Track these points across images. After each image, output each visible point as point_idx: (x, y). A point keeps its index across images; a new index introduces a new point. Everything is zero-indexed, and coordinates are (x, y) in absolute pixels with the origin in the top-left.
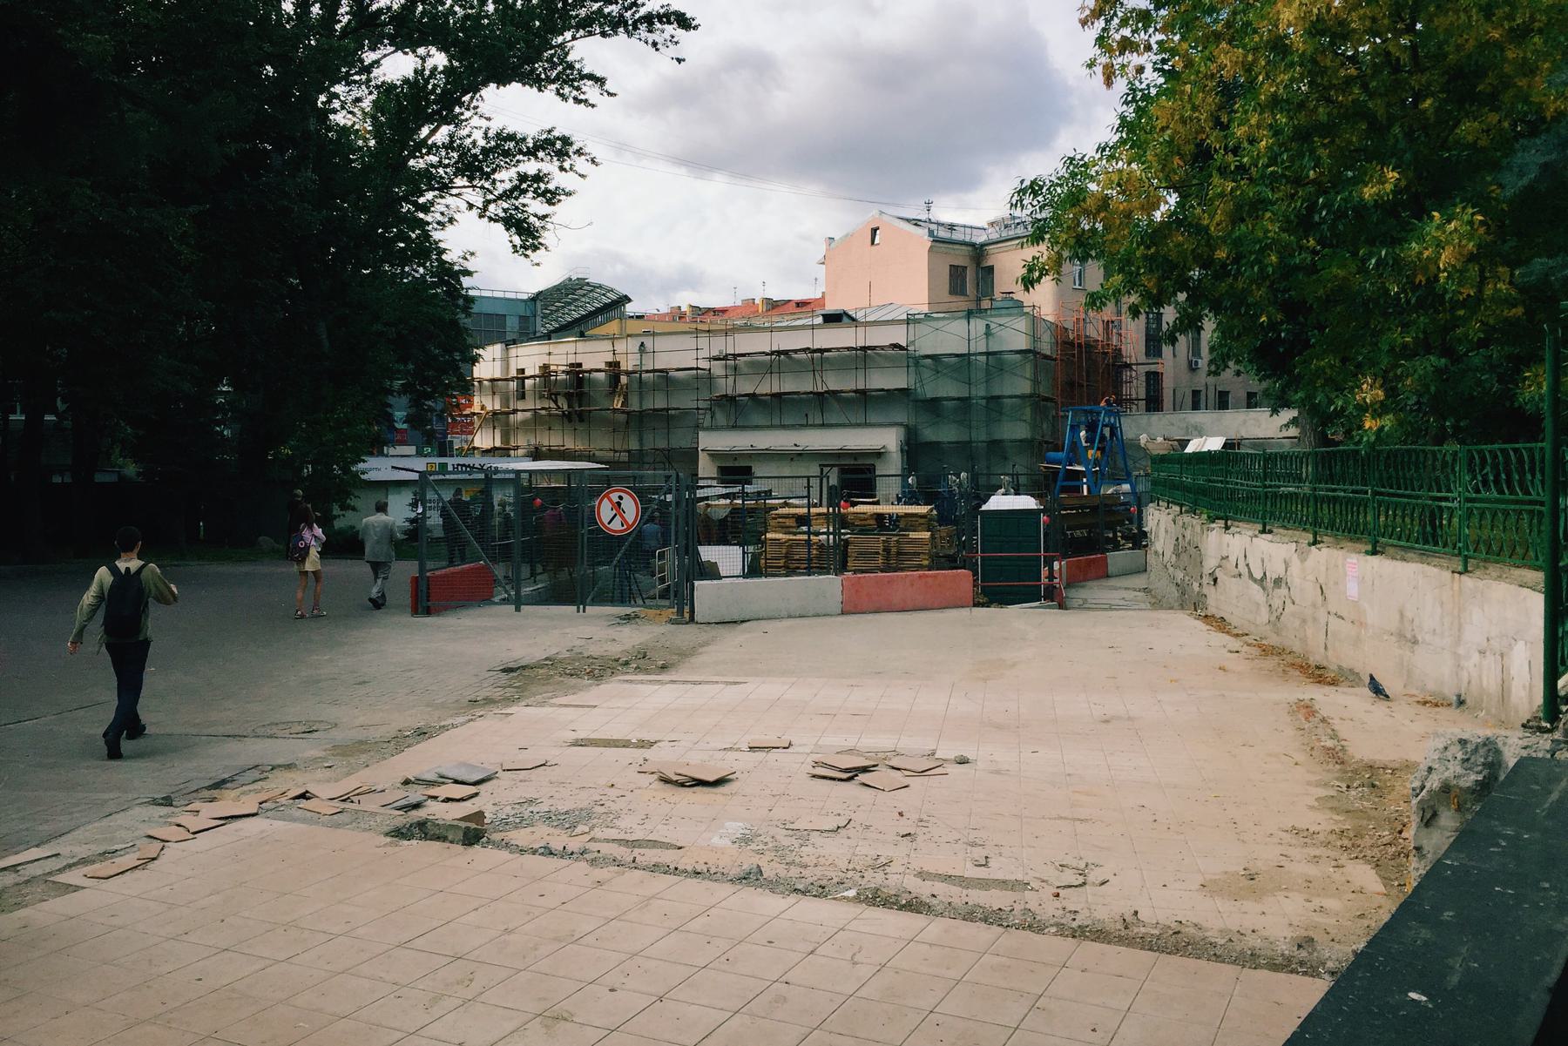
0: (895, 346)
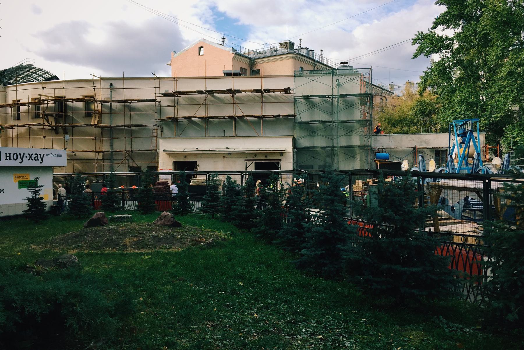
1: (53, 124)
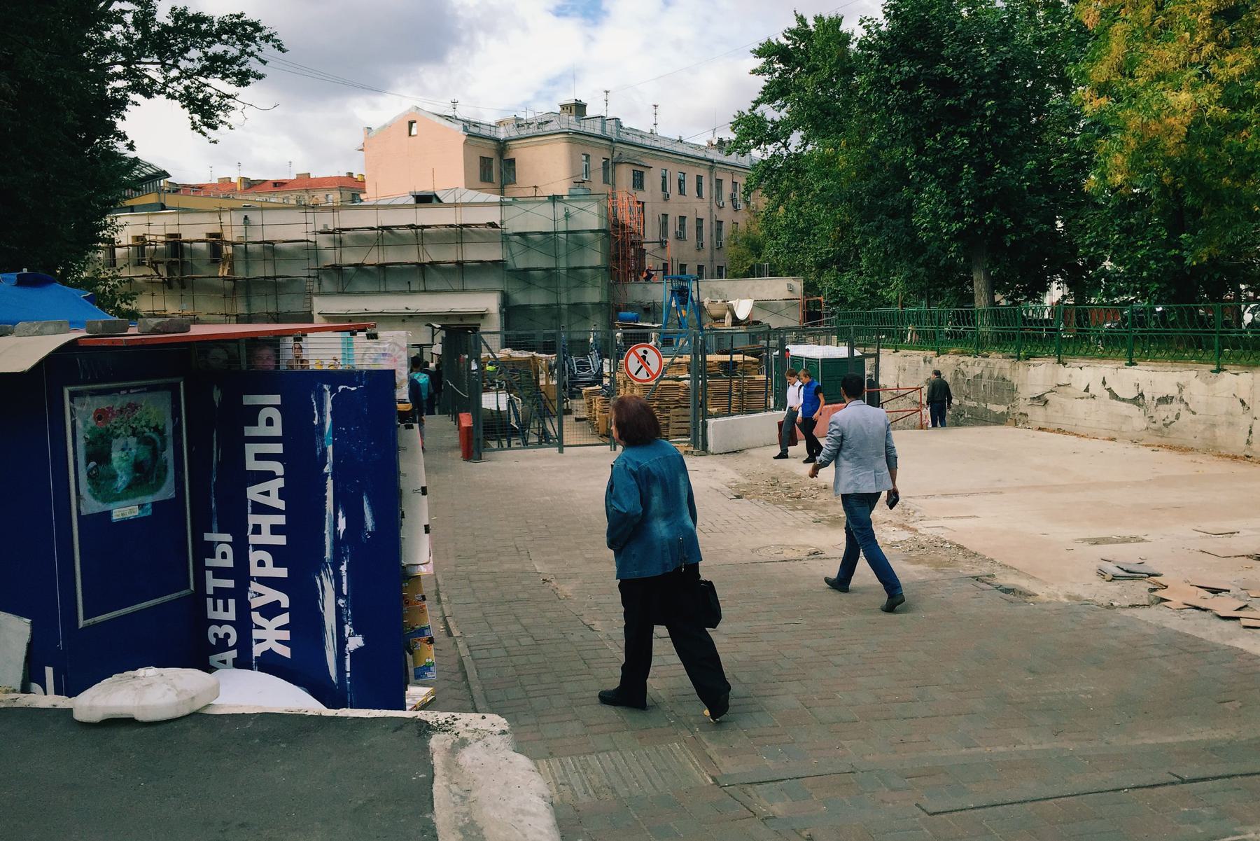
0: (493, 225)
1: (165, 275)
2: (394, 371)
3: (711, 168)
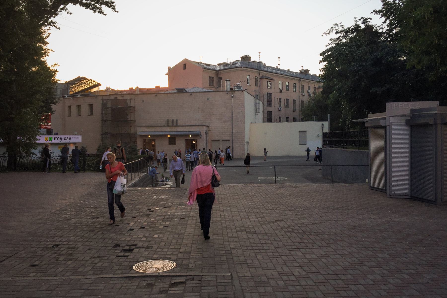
2: (175, 144)
3: (300, 81)
